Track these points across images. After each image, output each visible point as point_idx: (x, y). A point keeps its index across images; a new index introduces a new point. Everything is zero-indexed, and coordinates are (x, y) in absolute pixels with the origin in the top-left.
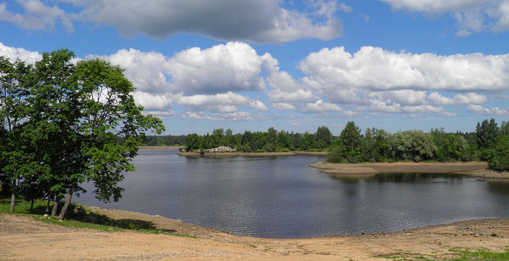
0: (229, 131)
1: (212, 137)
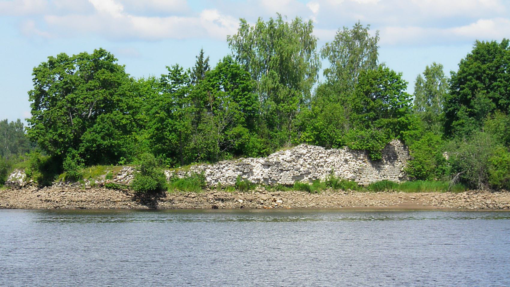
0: (356, 43)
1: (229, 74)
